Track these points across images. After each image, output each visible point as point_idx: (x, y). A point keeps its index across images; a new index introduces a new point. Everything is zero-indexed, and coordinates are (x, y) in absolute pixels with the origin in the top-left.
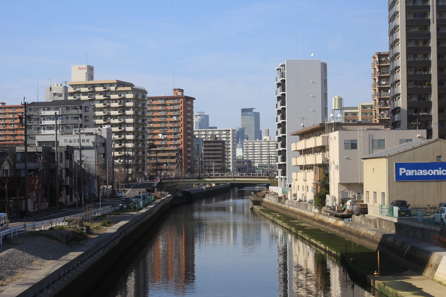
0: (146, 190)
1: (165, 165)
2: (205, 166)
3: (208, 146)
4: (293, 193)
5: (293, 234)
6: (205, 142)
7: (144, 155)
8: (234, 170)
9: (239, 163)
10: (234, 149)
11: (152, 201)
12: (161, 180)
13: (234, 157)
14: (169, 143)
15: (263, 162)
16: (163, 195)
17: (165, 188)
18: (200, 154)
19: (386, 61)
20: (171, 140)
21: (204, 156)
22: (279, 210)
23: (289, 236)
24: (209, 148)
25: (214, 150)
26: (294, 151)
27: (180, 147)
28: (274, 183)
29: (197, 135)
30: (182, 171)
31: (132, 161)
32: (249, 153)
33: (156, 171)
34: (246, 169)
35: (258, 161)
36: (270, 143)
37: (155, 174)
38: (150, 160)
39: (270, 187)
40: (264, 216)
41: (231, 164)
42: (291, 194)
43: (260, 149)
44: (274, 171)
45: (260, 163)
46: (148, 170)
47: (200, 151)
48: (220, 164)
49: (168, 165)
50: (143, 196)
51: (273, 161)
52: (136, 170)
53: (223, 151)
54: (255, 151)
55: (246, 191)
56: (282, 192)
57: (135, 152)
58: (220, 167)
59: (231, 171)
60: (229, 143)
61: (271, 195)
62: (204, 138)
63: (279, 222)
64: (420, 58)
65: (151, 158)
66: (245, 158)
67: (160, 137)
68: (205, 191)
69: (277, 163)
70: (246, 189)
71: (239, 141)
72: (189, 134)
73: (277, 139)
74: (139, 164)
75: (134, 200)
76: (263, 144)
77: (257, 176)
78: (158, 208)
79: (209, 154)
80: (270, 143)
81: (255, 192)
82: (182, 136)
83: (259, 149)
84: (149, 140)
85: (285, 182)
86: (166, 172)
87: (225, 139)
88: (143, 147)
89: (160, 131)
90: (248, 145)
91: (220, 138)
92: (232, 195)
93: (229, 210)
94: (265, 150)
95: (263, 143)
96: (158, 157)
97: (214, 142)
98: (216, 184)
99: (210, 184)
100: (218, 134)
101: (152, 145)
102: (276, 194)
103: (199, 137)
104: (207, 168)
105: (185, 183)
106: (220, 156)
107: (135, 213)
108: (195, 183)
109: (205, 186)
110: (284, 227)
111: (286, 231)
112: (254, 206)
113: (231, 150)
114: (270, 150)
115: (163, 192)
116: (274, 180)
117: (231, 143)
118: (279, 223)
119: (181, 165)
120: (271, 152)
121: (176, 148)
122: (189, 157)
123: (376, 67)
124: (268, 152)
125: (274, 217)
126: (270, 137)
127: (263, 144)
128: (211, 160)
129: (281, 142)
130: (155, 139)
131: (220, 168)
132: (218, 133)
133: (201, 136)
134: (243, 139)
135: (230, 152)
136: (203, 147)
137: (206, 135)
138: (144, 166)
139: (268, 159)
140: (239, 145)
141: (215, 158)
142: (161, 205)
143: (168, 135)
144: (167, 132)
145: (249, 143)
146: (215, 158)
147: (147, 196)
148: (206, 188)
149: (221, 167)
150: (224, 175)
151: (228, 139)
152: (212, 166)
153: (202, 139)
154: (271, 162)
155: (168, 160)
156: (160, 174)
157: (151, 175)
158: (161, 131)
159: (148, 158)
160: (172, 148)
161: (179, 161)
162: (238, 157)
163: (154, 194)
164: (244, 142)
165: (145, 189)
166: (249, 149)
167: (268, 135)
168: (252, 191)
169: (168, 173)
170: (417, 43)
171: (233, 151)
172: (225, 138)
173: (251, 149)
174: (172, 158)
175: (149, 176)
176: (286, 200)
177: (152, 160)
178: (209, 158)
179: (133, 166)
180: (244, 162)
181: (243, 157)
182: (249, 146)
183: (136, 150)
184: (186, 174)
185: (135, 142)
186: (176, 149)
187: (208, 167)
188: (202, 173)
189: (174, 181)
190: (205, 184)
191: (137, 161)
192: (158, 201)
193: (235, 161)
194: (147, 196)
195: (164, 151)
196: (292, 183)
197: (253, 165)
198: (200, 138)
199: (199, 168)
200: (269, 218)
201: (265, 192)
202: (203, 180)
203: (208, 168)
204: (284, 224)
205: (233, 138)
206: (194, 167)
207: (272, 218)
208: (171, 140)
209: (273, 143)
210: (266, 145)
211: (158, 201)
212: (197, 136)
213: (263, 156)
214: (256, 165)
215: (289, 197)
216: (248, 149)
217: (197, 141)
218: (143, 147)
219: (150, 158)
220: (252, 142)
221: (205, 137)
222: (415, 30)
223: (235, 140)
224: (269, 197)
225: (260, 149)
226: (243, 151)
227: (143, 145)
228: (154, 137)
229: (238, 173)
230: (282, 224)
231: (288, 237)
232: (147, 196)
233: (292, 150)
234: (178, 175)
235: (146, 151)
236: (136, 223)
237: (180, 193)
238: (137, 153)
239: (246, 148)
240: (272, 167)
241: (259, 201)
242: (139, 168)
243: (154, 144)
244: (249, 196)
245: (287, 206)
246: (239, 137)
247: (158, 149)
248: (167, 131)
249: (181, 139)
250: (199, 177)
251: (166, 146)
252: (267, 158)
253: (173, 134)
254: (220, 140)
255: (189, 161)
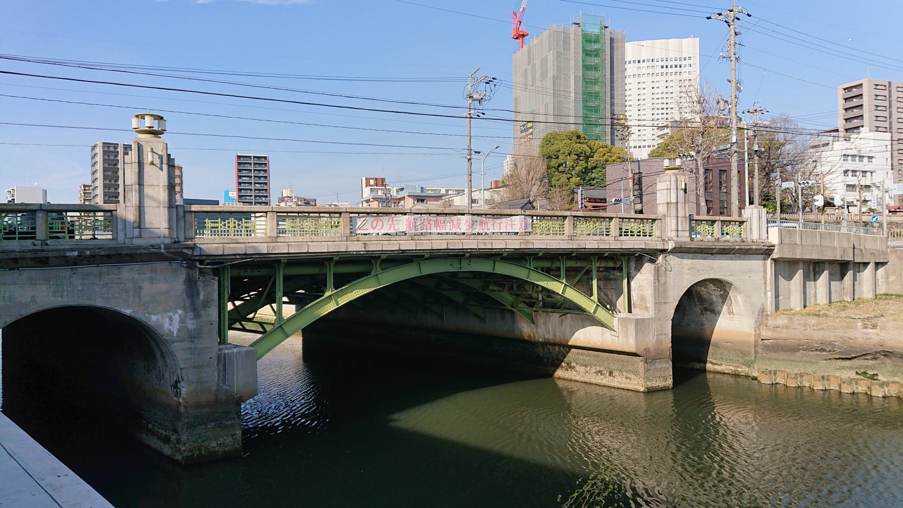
19: (89, 190)
64: (112, 190)
123: (82, 193)
170: (110, 181)
222: (109, 173)
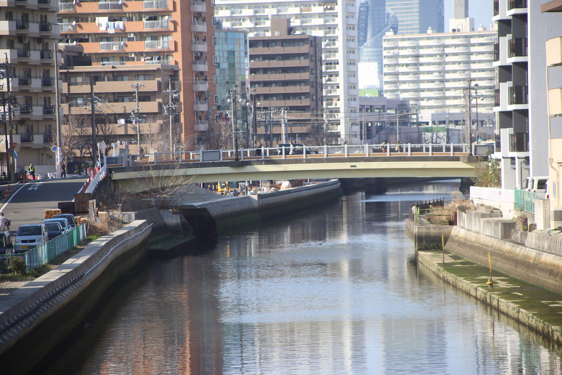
0: (60, 206)
1: (122, 121)
2: (256, 124)
3: (266, 57)
4: (552, 209)
5: (556, 346)
6: (253, 43)
7: (47, 88)
8: (351, 135)
9: (367, 110)
10: (351, 63)
11: (79, 243)
12: (109, 171)
13: (353, 92)
14: (134, 46)
15: (450, 106)
16: (118, 221)
17: (123, 198)
18: (238, 83)
20: (141, 36)
21: (250, 91)
22: (502, 266)
23: (545, 354)
24: (266, 64)
25: (285, 70)
26: (555, 65)
27: (171, 61)
28: (486, 174)
29: (228, 19)
30: (179, 142)
31: (10, 109)
32: (402, 78)
33: (92, 141)
34: (392, 131)
35: (432, 103)
36: (473, 41)
37: (87, 152)
38: (70, 106)
39: (472, 188)
40: (455, 287)
41: (341, 116)
42: (545, 211)
43: (439, 64)
44: (485, 135)
45: (439, 111)
46: (63, 140)
47: (237, 72)
48: (306, 115)
49: (131, 122)
50: (48, 227)
51: (484, 102)
52: (23, 140)
53: (314, 72)
54: (422, 68)
55: (392, 205)
56: (516, 204)
57: (16, 80)
58: (305, 125)
59: (343, 136)
60: (334, 44)
61: (477, 214)
62: (251, 30)
63: (508, 306)
65: (72, 99)
66: (388, 96)
67: (102, 29)
68: (256, 205)
69: (497, 109)
70: (391, 197)
71: (365, 37)
72: (198, 16)
73: (496, 27)
74: (33, 118)
75: (17, 241)
76: (447, 46)
77: (430, 154)
78: (100, 266)
79: (267, 84)
80: (473, 41)
81: (424, 207)
82: (175, 23)
83: (434, 64)
84: (65, 38)
85: (525, 172)
86: (127, 147)
87: (319, 33)
88: (46, 61)
89: (101, 7)
90: (396, 51)
91: (304, 28)
92: (345, 219)
93: (336, 266)
94: (456, 67)
95: (447, 42)
96: (96, 94)
97: (283, 42)
98: (293, 183)
99: (271, 182)
100: (297, 16)
101: (75, 54)
102: (493, 212)
103: (233, 25)
104: (261, 130)
105: (190, 181)
106: (306, 89)
107: (20, 285)
108: (222, 180)
109: (256, 191)
110: (524, 325)
111: (533, 336)
112: (421, 253)
113: (340, 68)
114: (473, 66)
115: (117, 214)
116: (488, 166)
117: (339, 44)
118: (505, 310)
119: (177, 119)
120: (475, 71)
121: (159, 66)
122: (201, 95)
124: (464, 71)
125: (489, 291)
126: (472, 21)
127: (447, 46)
128: (275, 103)
129: (509, 37)
130: (84, 35)
131: (304, 129)
132: (297, 10)
133: (241, 24)
134: (379, 31)
135: (335, 27)
136: (247, 60)
137: (256, 19)
138: (50, 126)
139: (464, 97)
140: (366, 50)
141: (286, 96)
142: (110, 255)
143: (130, 19)
144: (125, 10)
145: (401, 44)
146: (286, 96)
147: (64, 226)
148: (259, 196)
149: (309, 127)
150: (317, 152)
151: (329, 32)
152: (278, 124)
153: (245, 33)
154: (477, 106)
155: (130, 106)
156: (107, 151)
157: (75, 157)
158: (106, 7)
159: (64, 98)
160: (143, 64)
161: (168, 109)
162: (365, 91)
163: (85, 219)
164: (385, 40)
165: (55, 203)
166: (403, 65)
167: (466, 16)
168: (412, 204)
169: (134, 149)
171: (349, 95)
172: (320, 27)
173: (407, 65)
174: (145, 97)
175: (68, 158)
176: (529, 233)
177: (77, 105)
178: (267, 97)
179: (12, 128)
180: (384, 106)
181: (381, 92)
182: (402, 52)
183: (20, 72)
184: (192, 150)
185: (17, 45)
186: (158, 70)
187: (266, 127)
188: (247, 146)
189: (153, 173)
190: (256, 184)
191: (26, 110)
192: (101, 242)
193: (356, 104)
194: (64, 226)
195: (116, 76)
196: (548, 175)
197: (415, 117)
198: (236, 31)
199: (237, 130)
200: (473, 293)
201: (457, 205)
202: (248, 169)
203: (266, 131)
204: (525, 315)
205: (348, 27)
206: (220, 126)
207: (481, 293)
208: (141, 36)
209: (482, 40)
210: (457, 50)
211: (101, 242)
212: (226, 25)
213: (448, 85)
214: (426, 116)
215: (539, 220)
216: (398, 65)
217: (226, 40)
218: (46, 61)
219: (70, 98)
220: (409, 39)
221: (251, 25)
223: (354, 33)
224: (470, 223)
225: (439, 64)
226: (381, 72)
227: (45, 53)
228: (81, 27)
229: (367, 146)
230: (518, 312)
231: (538, 357)
232: (64, 226)
233: (549, 62)
234: (167, 155)
235: (55, 73)
236: (26, 317)
237: (174, 213)
238: (24, 82)
239: (392, 62)
240: (479, 121)
241: (435, 237)
242: (32, 134)
243: (80, 53)
244: (402, 219)
245: (533, 254)
246: (366, 25)
247: (96, 67)
248: (126, 6)
249: (174, 34)
250: (237, 159)
251: (123, 57)
252: (462, 91)
253: (147, 17)
254: (303, 34)
255: (203, 107)
